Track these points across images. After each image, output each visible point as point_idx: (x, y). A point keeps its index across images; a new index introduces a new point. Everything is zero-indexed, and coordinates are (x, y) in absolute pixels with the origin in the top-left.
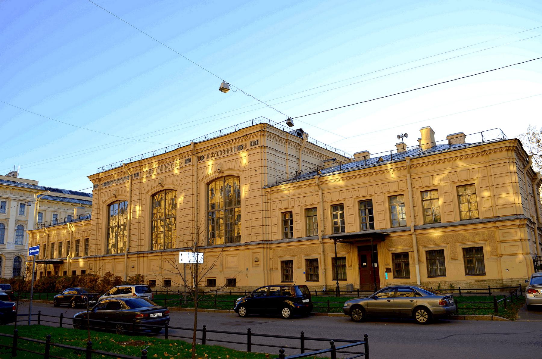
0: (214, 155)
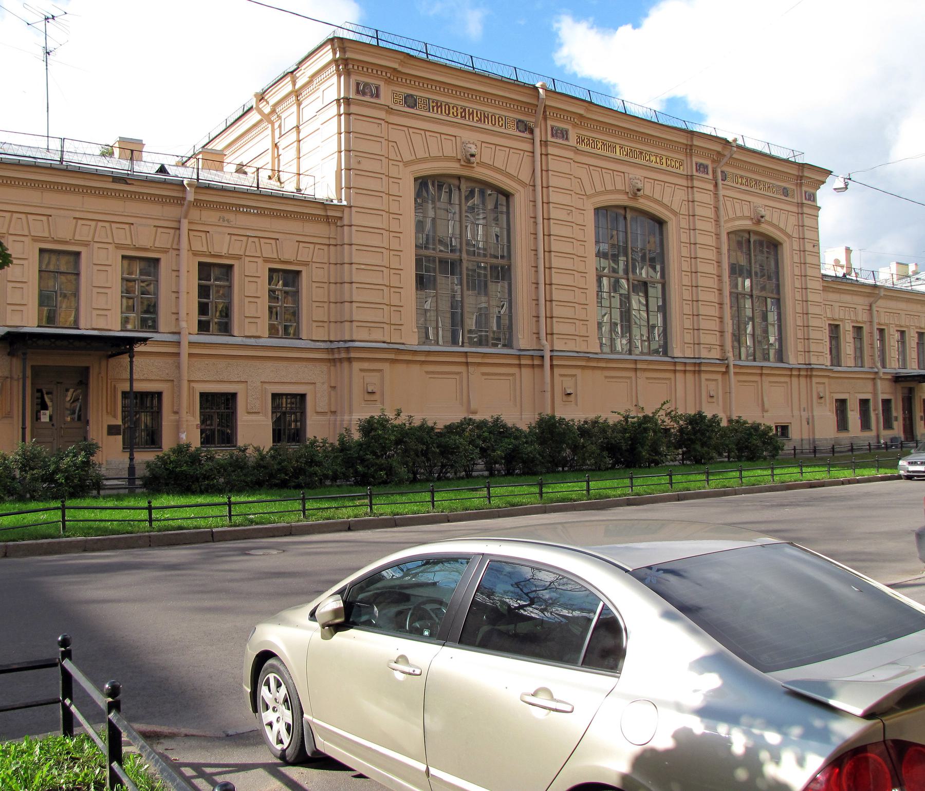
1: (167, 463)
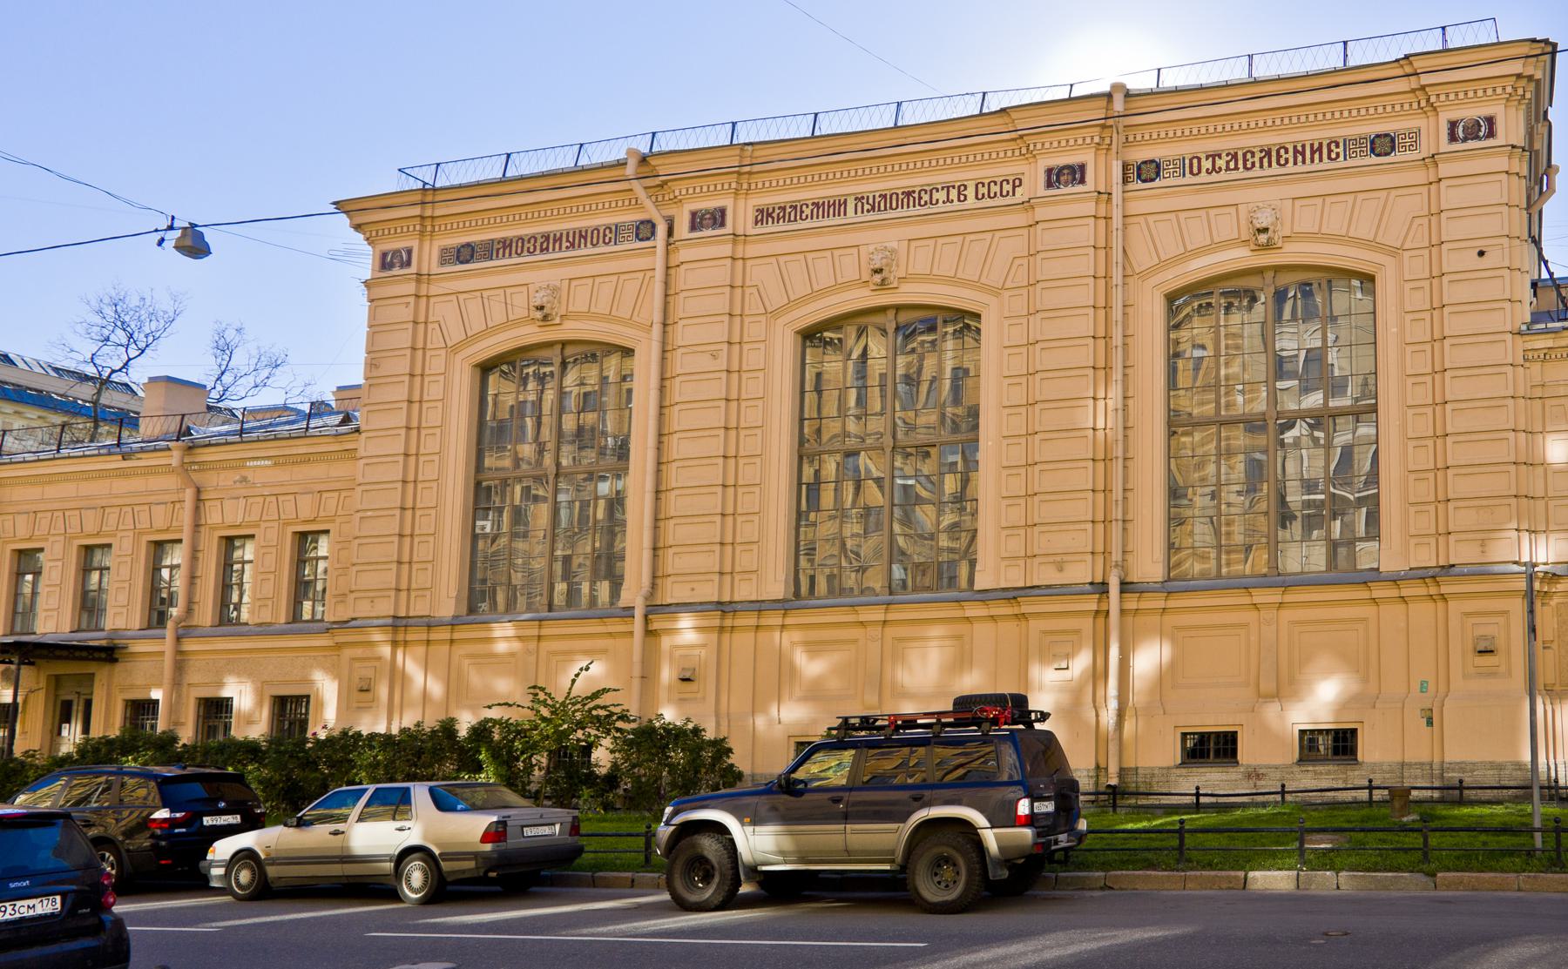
0: (1221, 163)
1: (193, 759)
